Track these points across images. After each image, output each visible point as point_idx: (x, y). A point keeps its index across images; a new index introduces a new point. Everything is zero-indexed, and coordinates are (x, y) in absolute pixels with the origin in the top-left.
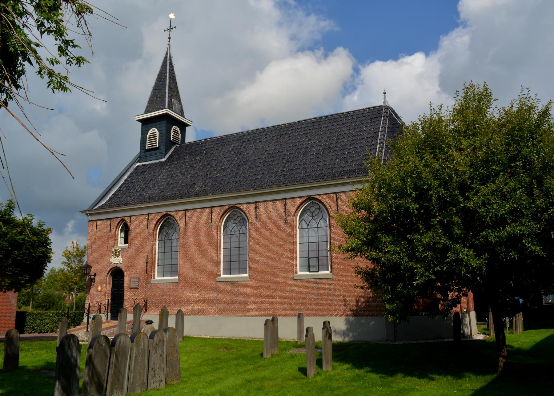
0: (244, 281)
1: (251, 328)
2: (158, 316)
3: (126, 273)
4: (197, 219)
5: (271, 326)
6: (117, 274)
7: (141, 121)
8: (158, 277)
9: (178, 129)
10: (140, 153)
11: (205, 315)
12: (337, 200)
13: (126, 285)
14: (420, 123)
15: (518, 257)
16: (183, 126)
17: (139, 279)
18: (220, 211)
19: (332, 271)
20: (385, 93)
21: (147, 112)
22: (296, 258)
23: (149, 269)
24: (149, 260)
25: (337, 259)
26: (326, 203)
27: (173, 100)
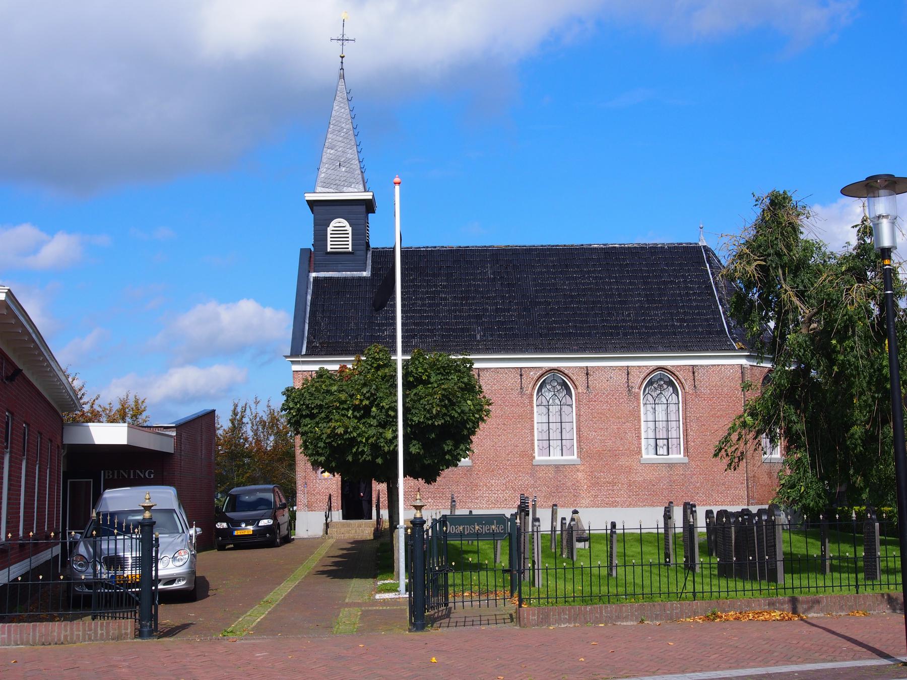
4: (498, 382)
8: (539, 455)
14: (745, 248)
15: (861, 451)
18: (534, 375)
25: (694, 442)
26: (680, 377)
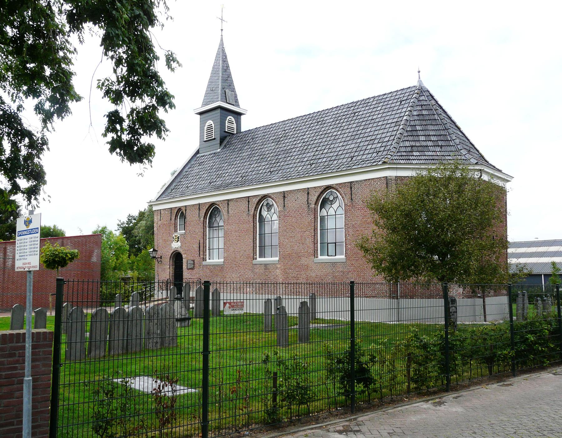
0: (273, 264)
2: (513, 235)
3: (184, 256)
6: (177, 257)
7: (201, 114)
9: (233, 120)
12: (351, 188)
13: (184, 267)
16: (238, 115)
17: (194, 261)
19: (346, 256)
20: (419, 72)
22: (317, 243)
23: (201, 253)
24: (201, 245)
27: (18, 180)
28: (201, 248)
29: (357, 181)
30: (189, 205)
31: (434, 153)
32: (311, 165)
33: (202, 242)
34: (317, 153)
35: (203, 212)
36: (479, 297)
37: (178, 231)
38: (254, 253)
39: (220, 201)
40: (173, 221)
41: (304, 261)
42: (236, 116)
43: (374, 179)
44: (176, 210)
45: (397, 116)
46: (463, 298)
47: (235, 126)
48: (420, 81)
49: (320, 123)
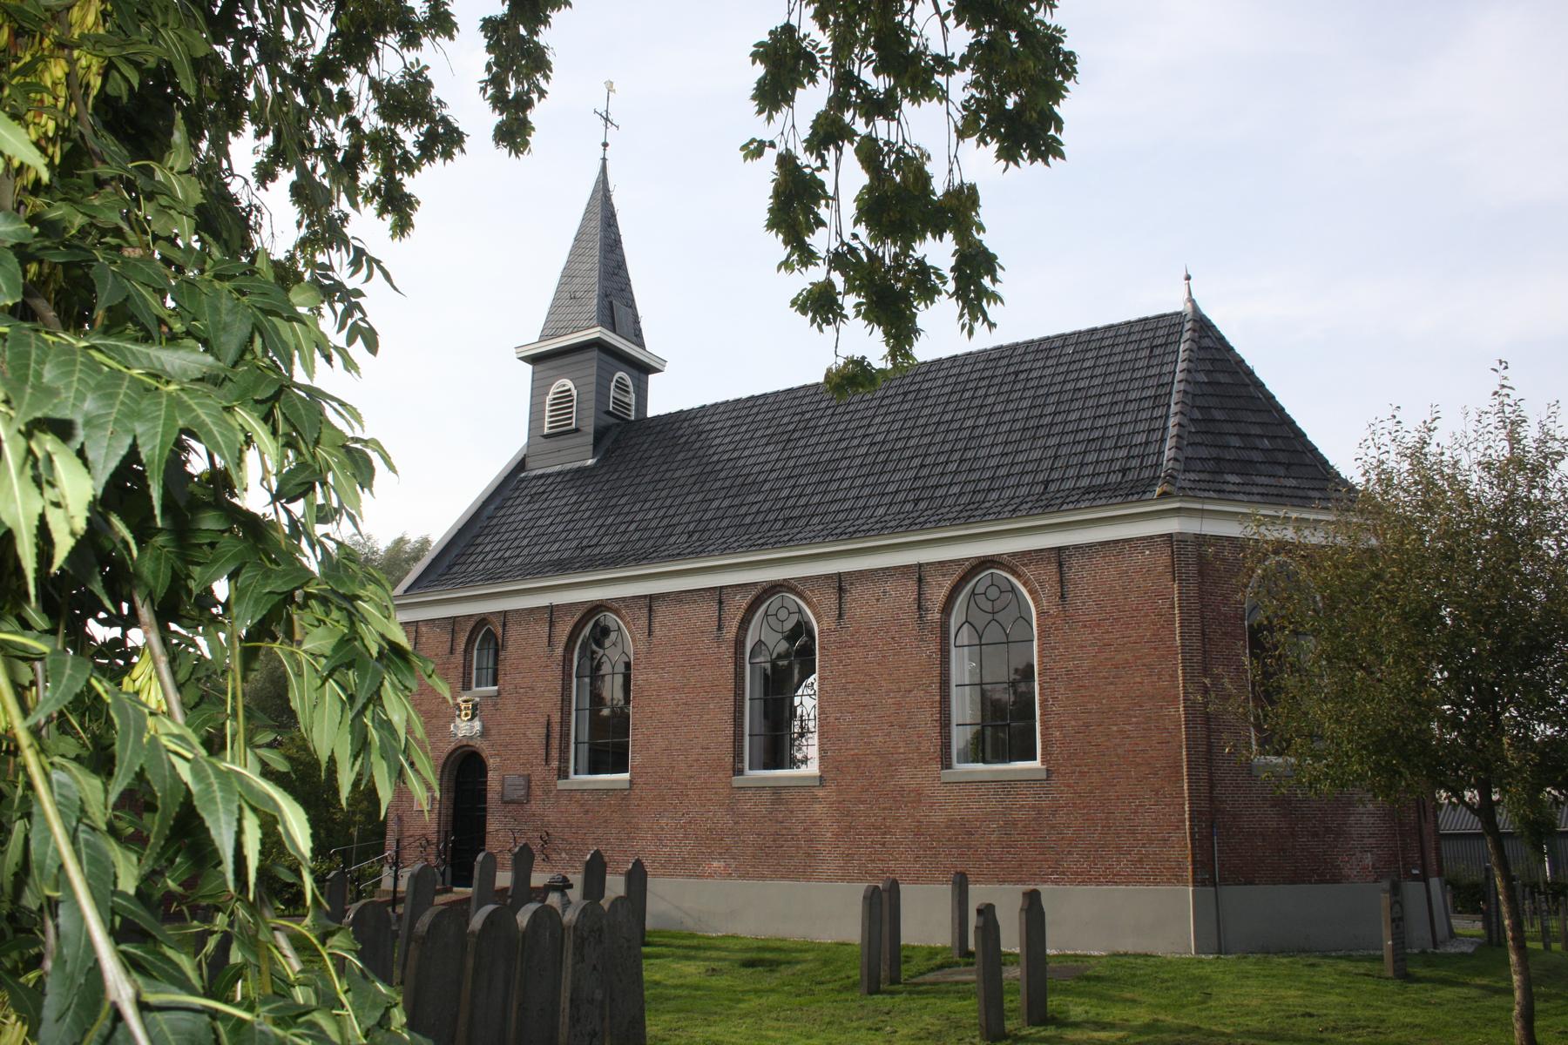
1: (828, 914)
3: (491, 762)
5: (882, 908)
7: (534, 360)
9: (629, 382)
10: (529, 445)
11: (698, 876)
16: (643, 370)
20: (1188, 278)
21: (543, 338)
23: (555, 753)
24: (556, 729)
28: (555, 743)
29: (1076, 547)
30: (517, 611)
31: (1272, 481)
32: (917, 501)
33: (556, 718)
34: (925, 472)
35: (564, 629)
36: (1416, 878)
37: (475, 689)
38: (738, 755)
39: (624, 599)
40: (459, 658)
41: (906, 778)
42: (635, 373)
43: (1131, 540)
44: (472, 623)
45: (1154, 382)
46: (1376, 881)
47: (632, 399)
48: (1192, 300)
49: (910, 396)
